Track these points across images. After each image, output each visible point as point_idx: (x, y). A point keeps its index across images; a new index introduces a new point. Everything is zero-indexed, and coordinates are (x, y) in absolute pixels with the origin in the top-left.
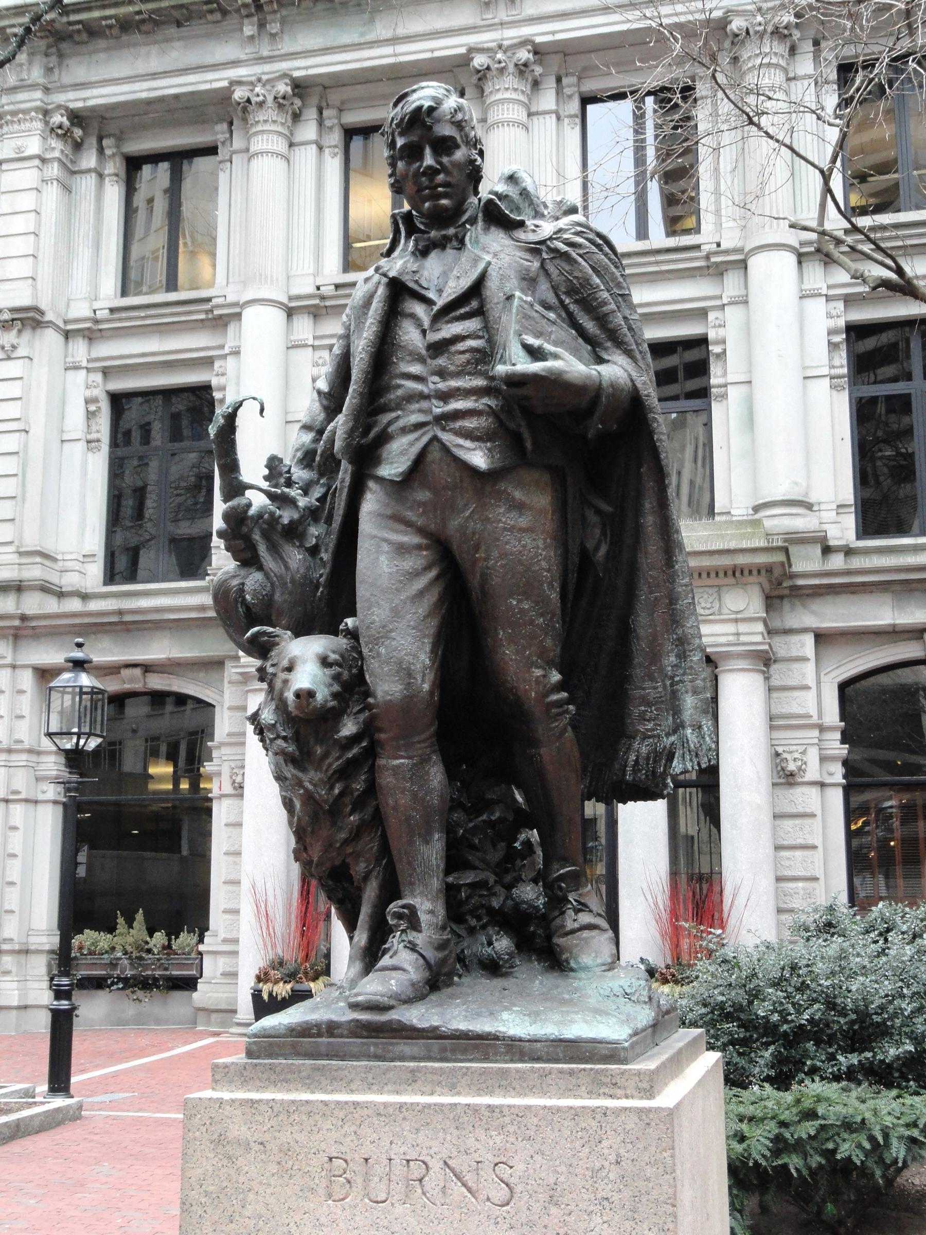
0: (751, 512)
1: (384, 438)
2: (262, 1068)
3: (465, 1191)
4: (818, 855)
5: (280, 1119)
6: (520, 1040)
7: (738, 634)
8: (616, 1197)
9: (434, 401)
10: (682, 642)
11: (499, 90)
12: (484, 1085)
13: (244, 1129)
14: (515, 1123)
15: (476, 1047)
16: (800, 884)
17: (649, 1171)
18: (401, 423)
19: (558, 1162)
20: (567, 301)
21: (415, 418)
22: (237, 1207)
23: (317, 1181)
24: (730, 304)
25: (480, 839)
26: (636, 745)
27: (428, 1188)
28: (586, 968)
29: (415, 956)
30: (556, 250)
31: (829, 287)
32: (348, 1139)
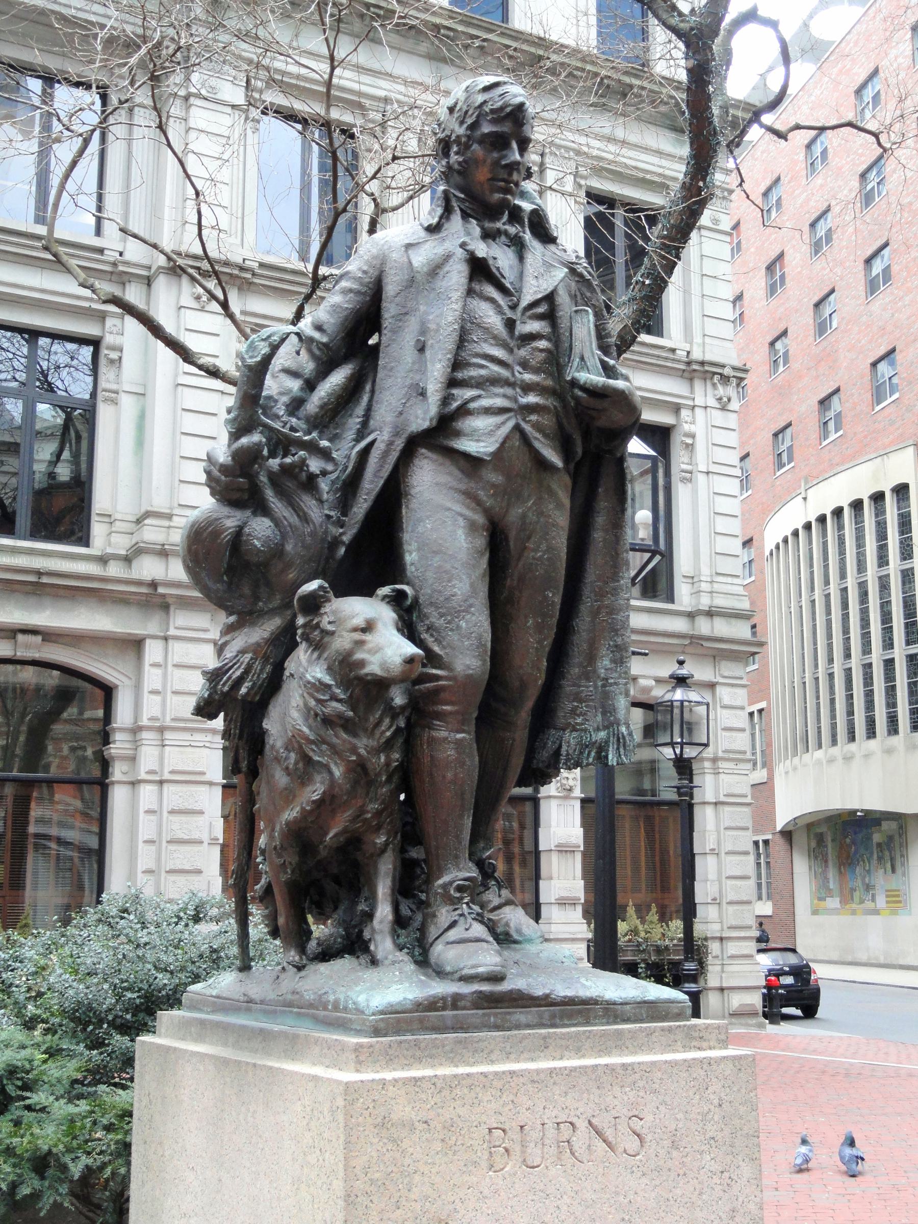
2: (407, 1045)
5: (443, 1094)
6: (615, 1003)
8: (719, 1136)
12: (603, 1047)
14: (644, 1078)
15: (580, 1012)
17: (742, 1109)
23: (479, 1154)
32: (507, 1109)
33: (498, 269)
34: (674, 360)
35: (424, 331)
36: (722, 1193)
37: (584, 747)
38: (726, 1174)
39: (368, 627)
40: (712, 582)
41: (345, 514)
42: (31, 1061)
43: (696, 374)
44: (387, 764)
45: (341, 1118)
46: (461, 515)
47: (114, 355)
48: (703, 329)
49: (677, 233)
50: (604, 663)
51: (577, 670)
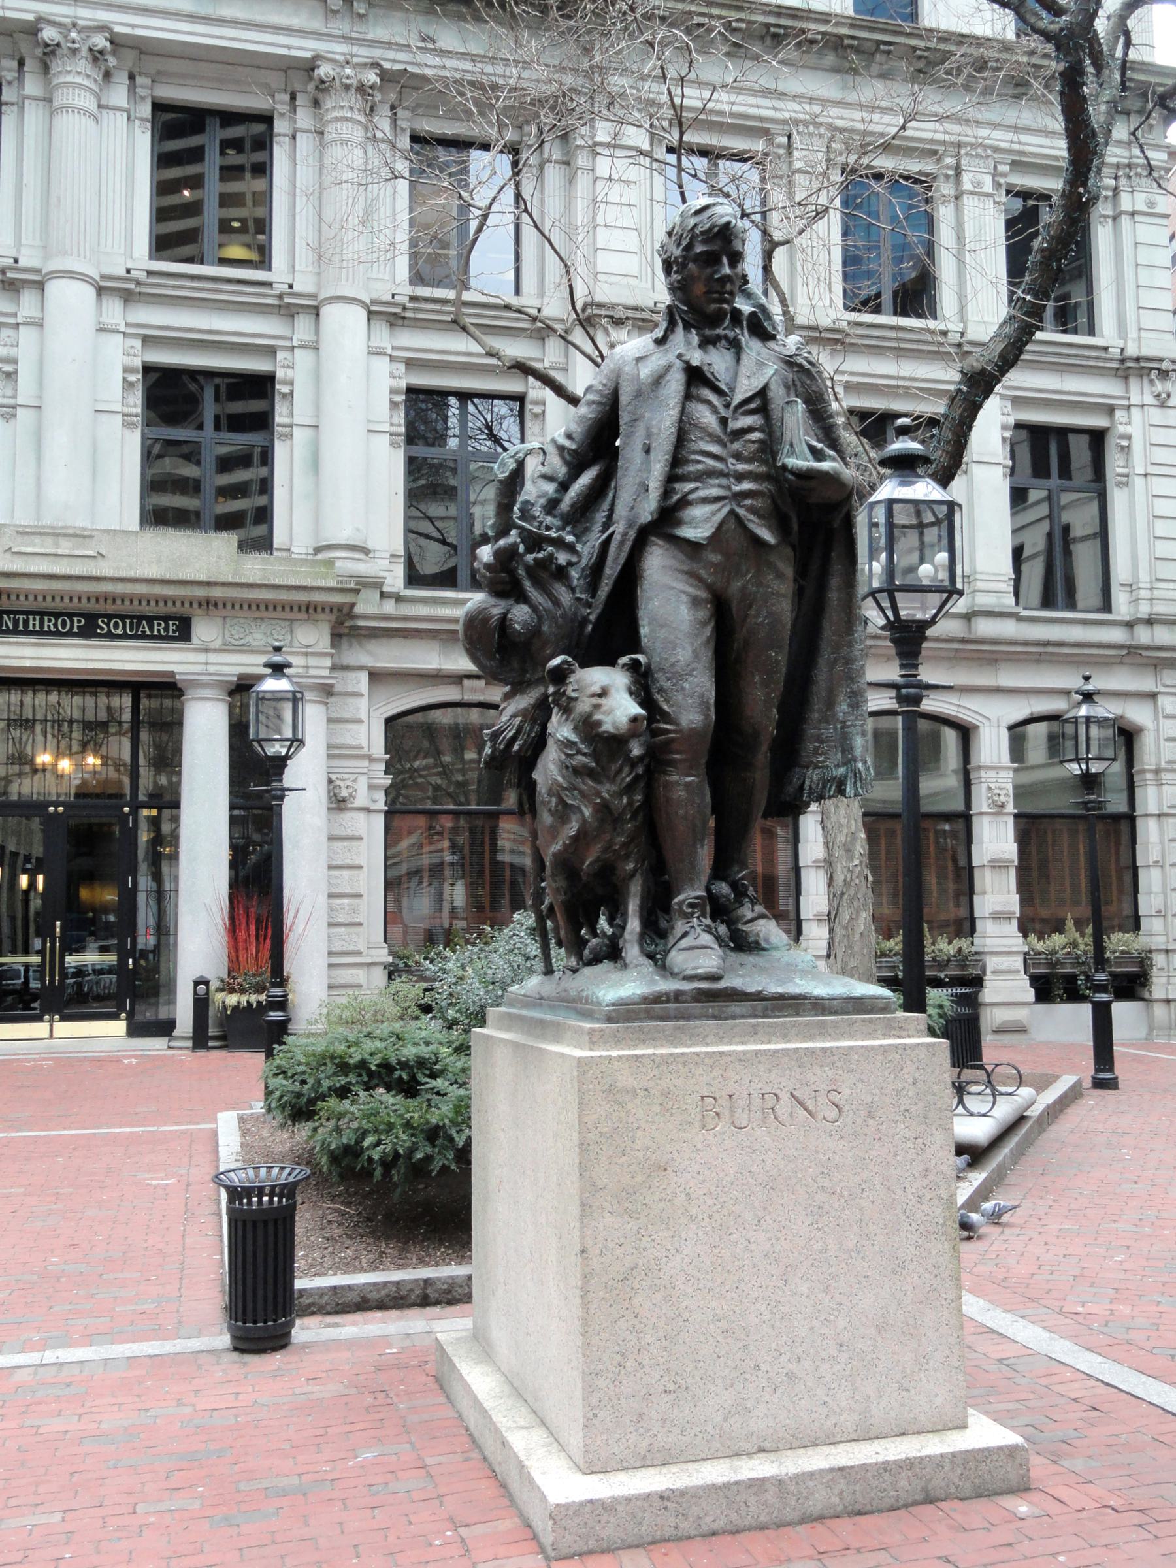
0: (311, 551)
4: (363, 874)
6: (822, 999)
7: (307, 667)
8: (913, 1109)
11: (69, 72)
13: (631, 1079)
15: (790, 1006)
16: (346, 901)
17: (936, 1088)
24: (300, 347)
27: (779, 1113)
31: (394, 348)
33: (712, 373)
34: (1105, 359)
35: (649, 435)
36: (915, 1156)
37: (825, 782)
38: (920, 1141)
39: (603, 693)
40: (1151, 589)
41: (593, 597)
42: (436, 1054)
43: (1131, 372)
44: (630, 803)
45: (576, 1084)
46: (684, 592)
47: (537, 409)
48: (1139, 322)
49: (1058, 244)
50: (843, 707)
51: (816, 715)
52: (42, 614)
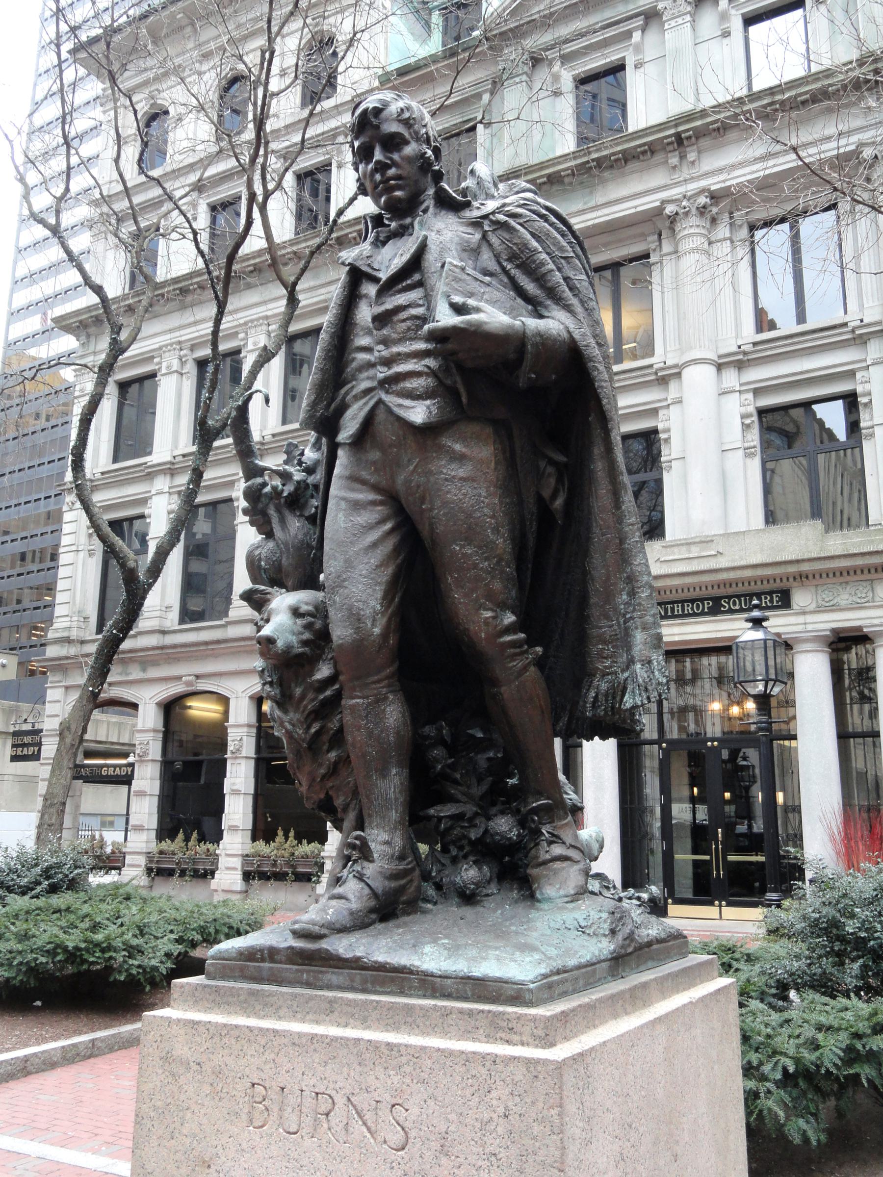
1: (343, 408)
3: (365, 1130)
6: (432, 975)
9: (378, 367)
10: (631, 579)
12: (391, 1021)
15: (393, 980)
17: (536, 1129)
18: (354, 392)
19: (449, 1110)
20: (509, 267)
21: (365, 385)
22: (178, 1125)
24: (873, 364)
25: (462, 774)
26: (595, 683)
27: (333, 1124)
28: (549, 899)
29: (362, 885)
30: (497, 223)
52: (683, 602)
